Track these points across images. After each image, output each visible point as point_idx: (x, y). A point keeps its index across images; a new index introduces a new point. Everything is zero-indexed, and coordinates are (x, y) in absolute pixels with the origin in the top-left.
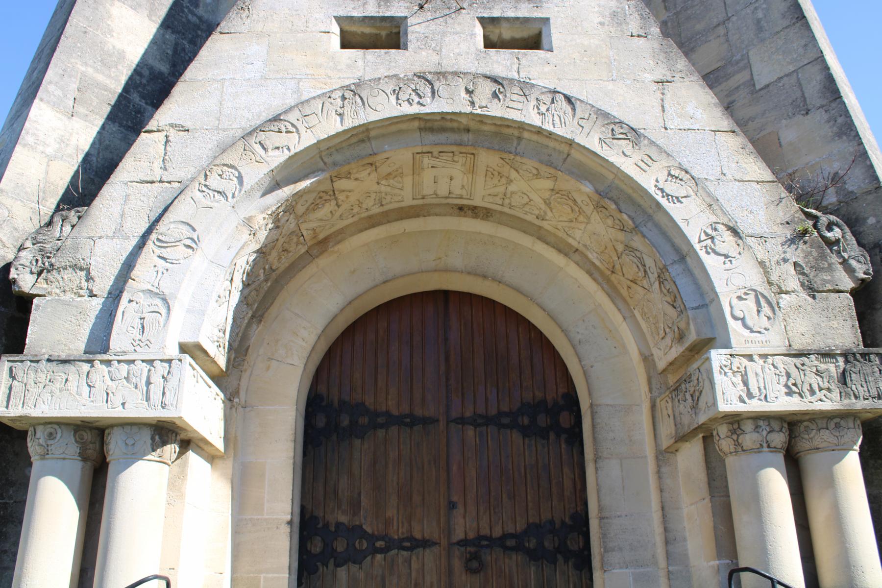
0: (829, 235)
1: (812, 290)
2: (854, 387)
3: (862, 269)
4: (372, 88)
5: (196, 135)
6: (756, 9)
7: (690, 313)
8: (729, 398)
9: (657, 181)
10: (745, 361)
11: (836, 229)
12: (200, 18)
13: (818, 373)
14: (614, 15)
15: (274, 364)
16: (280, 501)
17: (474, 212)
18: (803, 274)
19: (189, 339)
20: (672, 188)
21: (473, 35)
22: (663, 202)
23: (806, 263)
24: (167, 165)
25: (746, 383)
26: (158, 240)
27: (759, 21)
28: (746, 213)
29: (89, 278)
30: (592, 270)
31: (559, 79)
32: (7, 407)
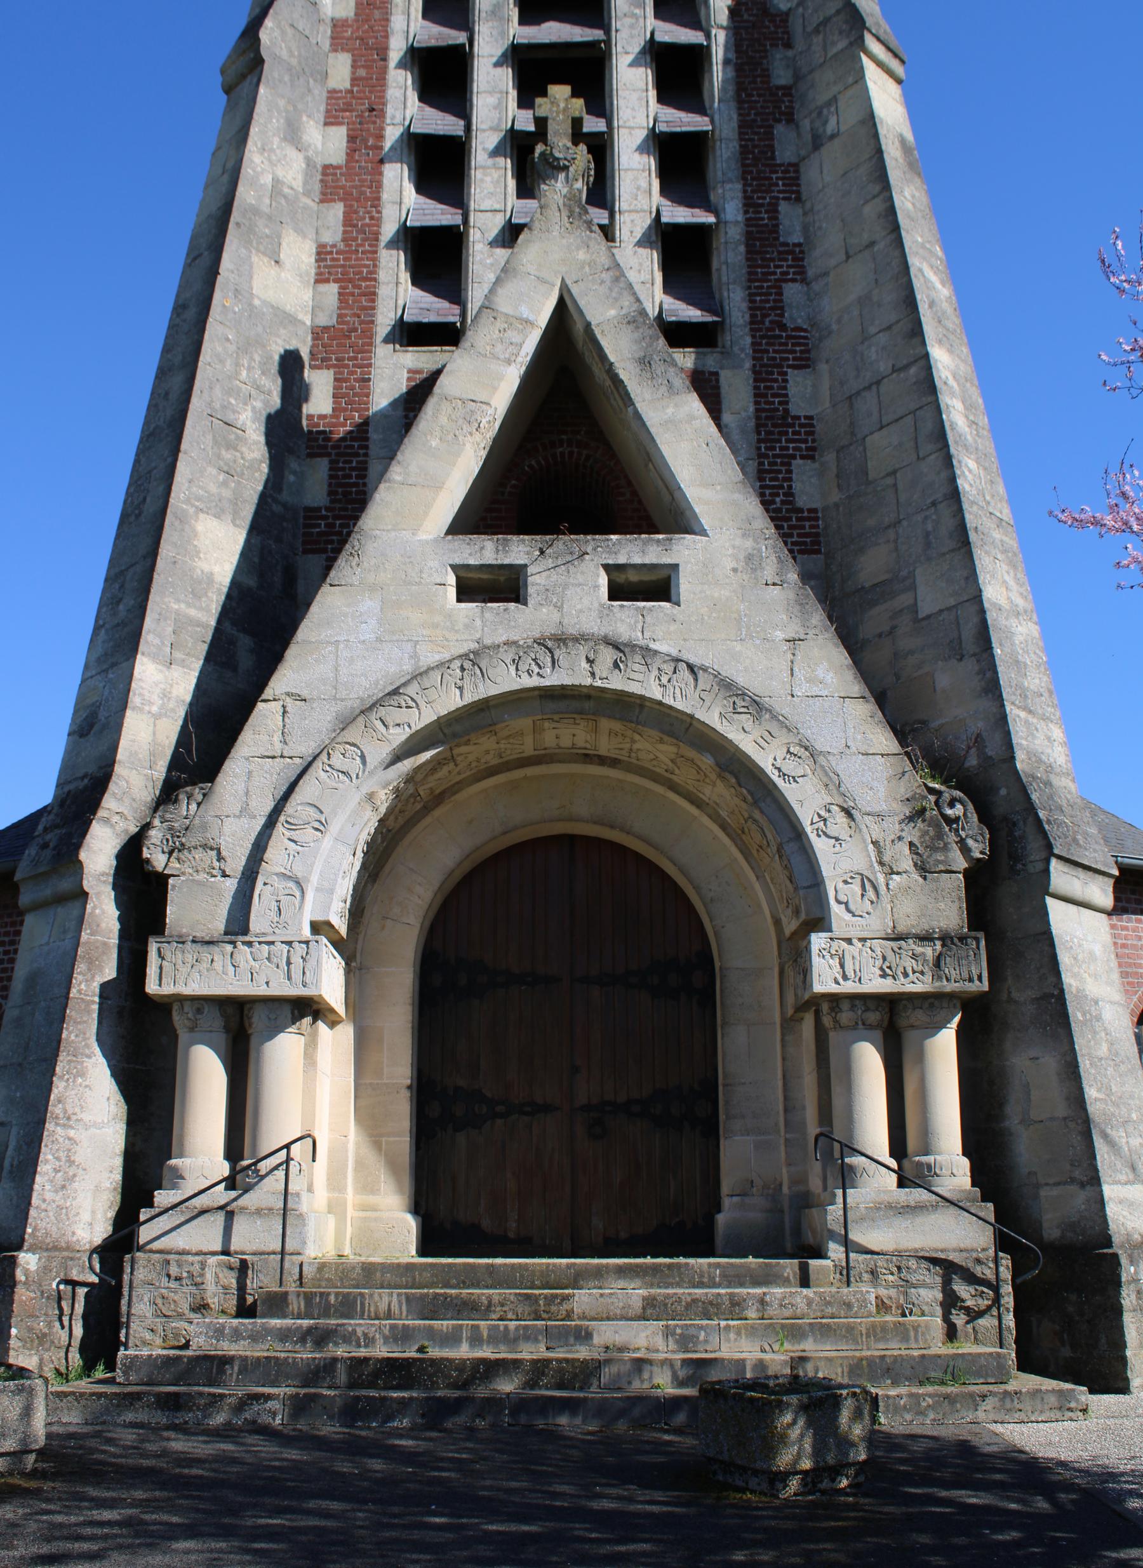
0: (949, 812)
1: (923, 869)
2: (947, 971)
3: (978, 849)
4: (491, 656)
5: (314, 705)
6: (926, 518)
7: (801, 892)
8: (825, 978)
9: (775, 759)
10: (844, 944)
11: (959, 806)
12: (285, 505)
13: (914, 956)
14: (749, 558)
15: (389, 923)
16: (399, 1068)
17: (602, 760)
18: (917, 854)
19: (319, 917)
20: (789, 766)
21: (597, 587)
22: (779, 782)
23: (922, 843)
24: (288, 738)
25: (842, 966)
26: (287, 822)
27: (927, 534)
28: (866, 789)
29: (220, 858)
30: (724, 827)
31: (685, 640)
32: (160, 985)
